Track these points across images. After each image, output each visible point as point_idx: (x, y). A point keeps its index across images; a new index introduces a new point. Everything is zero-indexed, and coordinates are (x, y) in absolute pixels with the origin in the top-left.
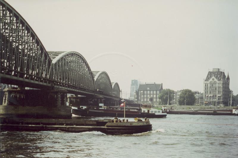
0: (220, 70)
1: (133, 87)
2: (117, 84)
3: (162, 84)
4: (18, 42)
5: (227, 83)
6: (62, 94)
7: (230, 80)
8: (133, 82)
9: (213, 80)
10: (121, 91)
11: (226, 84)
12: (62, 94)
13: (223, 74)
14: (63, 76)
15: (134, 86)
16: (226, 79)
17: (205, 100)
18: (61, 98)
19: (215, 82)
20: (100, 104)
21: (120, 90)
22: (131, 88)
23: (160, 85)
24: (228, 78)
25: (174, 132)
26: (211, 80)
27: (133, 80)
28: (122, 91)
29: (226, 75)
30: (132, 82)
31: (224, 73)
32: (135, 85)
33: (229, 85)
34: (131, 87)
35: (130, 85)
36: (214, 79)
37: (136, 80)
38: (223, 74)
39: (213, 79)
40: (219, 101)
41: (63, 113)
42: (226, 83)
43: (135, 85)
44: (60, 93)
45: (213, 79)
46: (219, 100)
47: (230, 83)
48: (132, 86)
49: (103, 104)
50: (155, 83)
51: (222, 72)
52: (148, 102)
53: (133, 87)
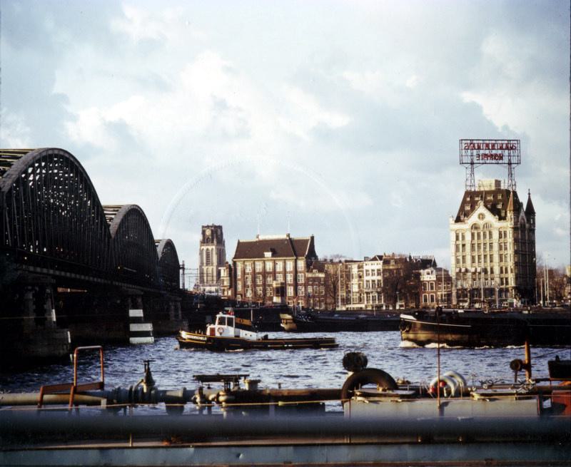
0: (502, 184)
1: (207, 249)
2: (170, 245)
3: (312, 238)
4: (38, 171)
5: (527, 225)
6: (37, 289)
7: (536, 217)
8: (208, 232)
9: (479, 218)
10: (183, 268)
11: (523, 231)
12: (37, 289)
13: (511, 199)
14: (37, 229)
15: (210, 248)
16: (522, 214)
17: (456, 286)
18: (34, 303)
19: (486, 226)
20: (142, 315)
21: (181, 263)
22: (201, 253)
23: (304, 242)
24: (530, 211)
25: (126, 360)
26: (474, 218)
27: (208, 227)
28: (185, 267)
29: (523, 199)
30: (204, 233)
31: (515, 194)
32: (215, 242)
33: (534, 233)
34: (201, 252)
35: (199, 243)
36: (479, 215)
37: (216, 227)
38: (511, 199)
39: (481, 214)
40: (504, 286)
41: (42, 350)
42: (525, 225)
43: (215, 242)
44: (30, 288)
45: (481, 216)
46: (502, 284)
47: (536, 228)
48: (205, 248)
49: (142, 311)
50: (288, 235)
51: (508, 192)
52: (271, 299)
53: (207, 249)
